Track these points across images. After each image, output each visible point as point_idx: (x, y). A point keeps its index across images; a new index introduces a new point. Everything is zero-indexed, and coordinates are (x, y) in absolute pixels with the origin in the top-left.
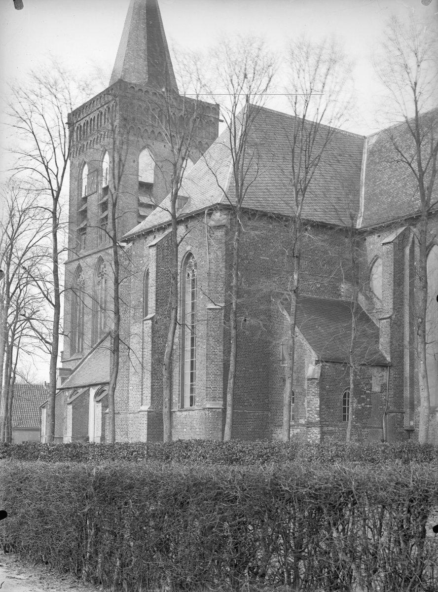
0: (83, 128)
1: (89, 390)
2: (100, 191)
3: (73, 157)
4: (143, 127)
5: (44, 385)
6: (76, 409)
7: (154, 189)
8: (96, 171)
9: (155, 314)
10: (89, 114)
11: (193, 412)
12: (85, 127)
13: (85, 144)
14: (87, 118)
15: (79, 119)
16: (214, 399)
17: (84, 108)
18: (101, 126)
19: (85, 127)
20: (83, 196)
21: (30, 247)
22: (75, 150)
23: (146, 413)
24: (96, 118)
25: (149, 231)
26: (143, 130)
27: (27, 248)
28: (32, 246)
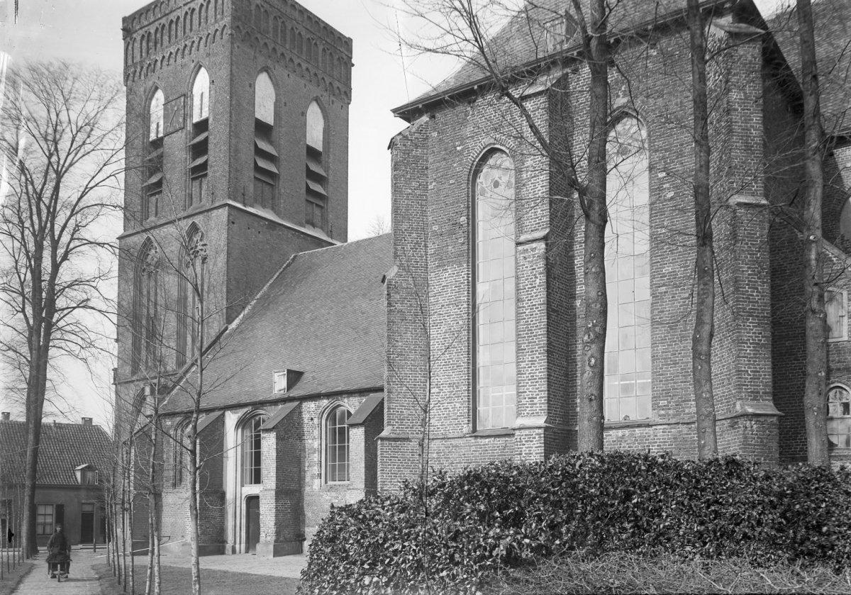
0: (153, 37)
1: (223, 415)
2: (189, 128)
3: (133, 81)
4: (262, 39)
5: (52, 425)
6: (283, 439)
7: (274, 133)
8: (180, 99)
9: (548, 230)
10: (168, 14)
11: (650, 431)
12: (159, 35)
13: (159, 59)
14: (163, 21)
15: (146, 23)
16: (755, 396)
17: (156, 6)
18: (191, 30)
19: (159, 35)
20: (153, 136)
21: (91, 188)
22: (138, 70)
23: (541, 431)
24: (182, 19)
25: (463, 92)
26: (262, 42)
27: (86, 188)
28: (96, 185)
